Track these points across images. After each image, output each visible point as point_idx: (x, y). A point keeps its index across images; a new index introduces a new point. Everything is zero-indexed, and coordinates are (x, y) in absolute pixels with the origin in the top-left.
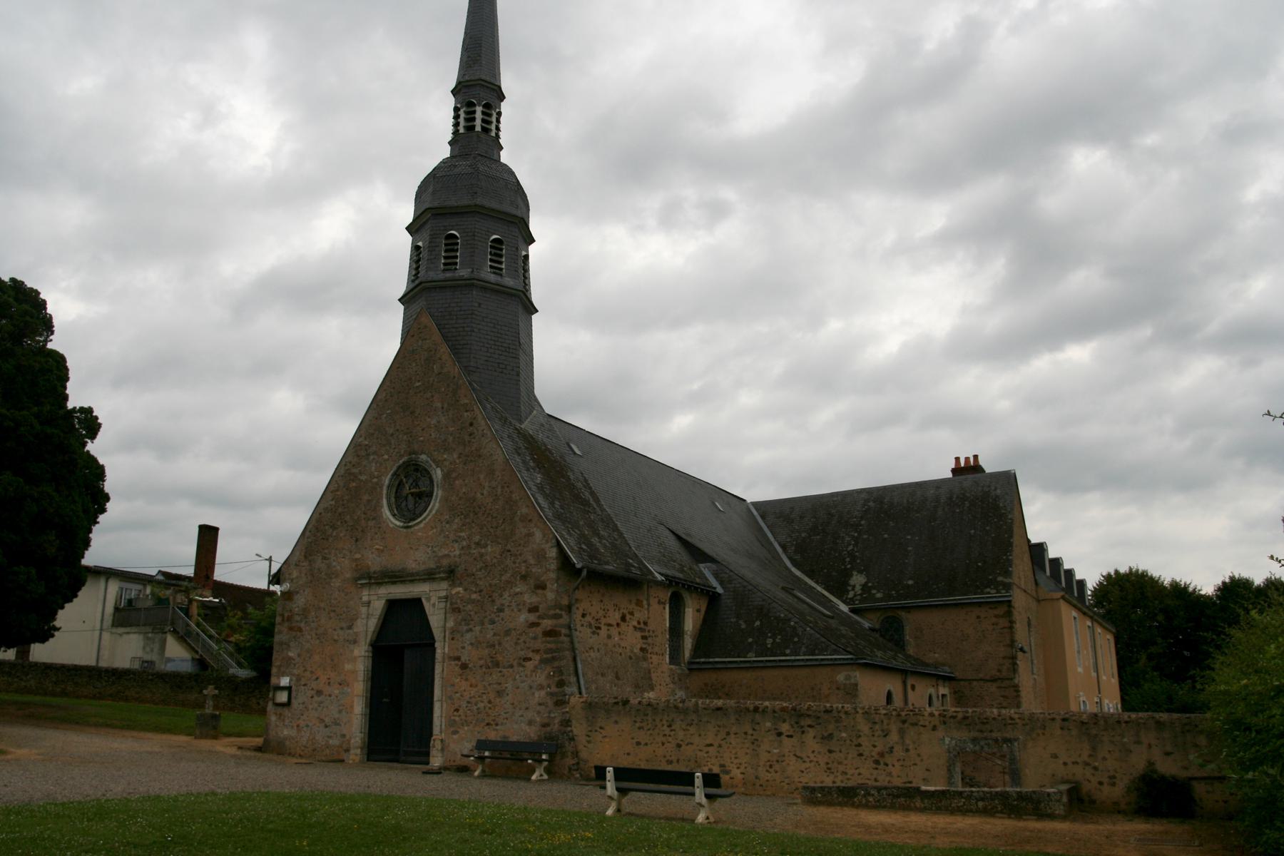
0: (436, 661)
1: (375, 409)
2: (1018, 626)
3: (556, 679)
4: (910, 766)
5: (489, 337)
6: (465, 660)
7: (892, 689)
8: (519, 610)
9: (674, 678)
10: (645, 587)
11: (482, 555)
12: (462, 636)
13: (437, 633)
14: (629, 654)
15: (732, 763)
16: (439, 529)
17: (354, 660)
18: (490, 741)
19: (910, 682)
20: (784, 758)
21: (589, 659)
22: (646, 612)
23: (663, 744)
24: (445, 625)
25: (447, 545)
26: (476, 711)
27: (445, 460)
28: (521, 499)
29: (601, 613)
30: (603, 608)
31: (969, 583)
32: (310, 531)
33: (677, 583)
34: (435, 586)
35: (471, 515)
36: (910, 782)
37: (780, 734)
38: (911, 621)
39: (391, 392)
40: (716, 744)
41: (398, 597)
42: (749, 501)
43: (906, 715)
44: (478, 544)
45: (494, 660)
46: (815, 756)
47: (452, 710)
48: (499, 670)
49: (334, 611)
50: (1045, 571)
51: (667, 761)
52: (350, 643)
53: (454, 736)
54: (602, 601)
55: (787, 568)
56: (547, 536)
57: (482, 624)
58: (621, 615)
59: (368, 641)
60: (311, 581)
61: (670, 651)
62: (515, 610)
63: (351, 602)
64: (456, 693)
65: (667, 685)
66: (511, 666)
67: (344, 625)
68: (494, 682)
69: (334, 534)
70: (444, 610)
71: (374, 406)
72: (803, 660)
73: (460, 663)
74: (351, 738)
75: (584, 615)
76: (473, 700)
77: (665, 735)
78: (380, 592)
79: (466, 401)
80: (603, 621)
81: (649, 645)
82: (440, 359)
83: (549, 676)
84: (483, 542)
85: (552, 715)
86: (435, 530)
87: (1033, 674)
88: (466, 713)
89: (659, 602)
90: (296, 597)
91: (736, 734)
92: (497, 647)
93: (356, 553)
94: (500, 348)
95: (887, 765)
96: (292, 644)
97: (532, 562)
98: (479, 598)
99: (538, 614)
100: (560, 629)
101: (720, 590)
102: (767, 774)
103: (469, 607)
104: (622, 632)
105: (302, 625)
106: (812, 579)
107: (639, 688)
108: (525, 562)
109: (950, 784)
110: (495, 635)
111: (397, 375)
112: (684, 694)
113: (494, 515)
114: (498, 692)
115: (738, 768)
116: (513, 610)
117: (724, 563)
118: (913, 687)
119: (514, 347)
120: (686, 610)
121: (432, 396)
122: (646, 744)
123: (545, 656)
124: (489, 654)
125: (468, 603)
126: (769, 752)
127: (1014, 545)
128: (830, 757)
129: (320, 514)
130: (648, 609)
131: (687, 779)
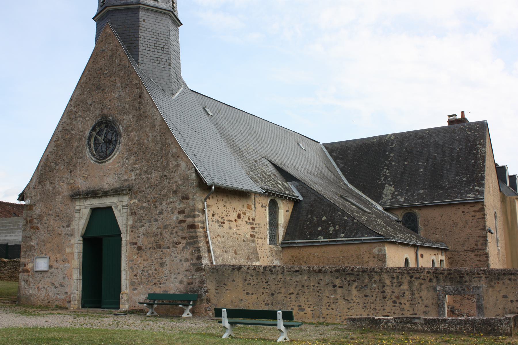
0: (122, 245)
1: (80, 89)
2: (488, 217)
3: (196, 255)
4: (415, 304)
5: (151, 41)
6: (140, 245)
7: (408, 257)
8: (173, 213)
9: (272, 253)
10: (253, 197)
11: (149, 179)
12: (138, 229)
13: (122, 228)
14: (243, 239)
15: (305, 304)
16: (121, 164)
17: (72, 246)
18: (157, 294)
19: (420, 252)
20: (337, 301)
21: (217, 242)
22: (254, 212)
23: (263, 293)
24: (127, 223)
25: (127, 173)
26: (147, 276)
27: (124, 120)
28: (172, 143)
29: (225, 213)
30: (226, 210)
31: (477, 194)
32: (42, 167)
33: (273, 194)
34: (120, 198)
35: (142, 154)
36: (416, 314)
37: (334, 286)
38: (422, 215)
39: (89, 78)
40: (295, 293)
41: (98, 206)
42: (321, 143)
43: (413, 273)
44: (146, 172)
45: (158, 244)
46: (356, 299)
47: (133, 275)
48: (161, 250)
49: (58, 216)
50: (506, 183)
51: (266, 304)
52: (69, 236)
53: (135, 292)
54: (225, 206)
55: (345, 184)
56: (189, 166)
57: (150, 221)
58: (237, 214)
59: (80, 234)
60: (44, 198)
61: (270, 235)
62: (170, 213)
63: (69, 210)
64: (135, 265)
65: (268, 257)
66: (169, 248)
67: (65, 225)
68: (158, 258)
69: (57, 168)
70: (126, 214)
71: (79, 86)
72: (352, 240)
73: (137, 246)
74: (71, 294)
75: (213, 215)
76: (146, 269)
77: (264, 288)
78: (86, 204)
79: (136, 82)
80: (226, 218)
81: (256, 233)
82: (120, 56)
83: (192, 254)
84: (149, 171)
85: (194, 277)
86: (119, 164)
87: (497, 246)
88: (142, 277)
89: (262, 206)
90: (34, 208)
91: (307, 286)
92: (159, 236)
93: (70, 179)
94: (158, 48)
95: (400, 303)
96: (33, 237)
97: (180, 182)
98: (148, 205)
99: (184, 215)
100: (198, 224)
101: (301, 198)
102: (327, 310)
103: (142, 211)
104: (238, 225)
105: (39, 225)
106: (360, 191)
107: (250, 259)
108: (176, 182)
109: (438, 313)
110: (158, 228)
111: (93, 67)
112: (279, 263)
113: (156, 153)
114: (161, 264)
115: (309, 307)
116: (168, 213)
117: (303, 181)
118: (422, 256)
119: (167, 47)
120: (280, 211)
121: (115, 80)
122: (252, 294)
123: (189, 241)
124: (155, 241)
125: (141, 209)
126: (328, 297)
127: (486, 167)
128: (365, 300)
129: (48, 155)
130: (255, 210)
131: (273, 315)
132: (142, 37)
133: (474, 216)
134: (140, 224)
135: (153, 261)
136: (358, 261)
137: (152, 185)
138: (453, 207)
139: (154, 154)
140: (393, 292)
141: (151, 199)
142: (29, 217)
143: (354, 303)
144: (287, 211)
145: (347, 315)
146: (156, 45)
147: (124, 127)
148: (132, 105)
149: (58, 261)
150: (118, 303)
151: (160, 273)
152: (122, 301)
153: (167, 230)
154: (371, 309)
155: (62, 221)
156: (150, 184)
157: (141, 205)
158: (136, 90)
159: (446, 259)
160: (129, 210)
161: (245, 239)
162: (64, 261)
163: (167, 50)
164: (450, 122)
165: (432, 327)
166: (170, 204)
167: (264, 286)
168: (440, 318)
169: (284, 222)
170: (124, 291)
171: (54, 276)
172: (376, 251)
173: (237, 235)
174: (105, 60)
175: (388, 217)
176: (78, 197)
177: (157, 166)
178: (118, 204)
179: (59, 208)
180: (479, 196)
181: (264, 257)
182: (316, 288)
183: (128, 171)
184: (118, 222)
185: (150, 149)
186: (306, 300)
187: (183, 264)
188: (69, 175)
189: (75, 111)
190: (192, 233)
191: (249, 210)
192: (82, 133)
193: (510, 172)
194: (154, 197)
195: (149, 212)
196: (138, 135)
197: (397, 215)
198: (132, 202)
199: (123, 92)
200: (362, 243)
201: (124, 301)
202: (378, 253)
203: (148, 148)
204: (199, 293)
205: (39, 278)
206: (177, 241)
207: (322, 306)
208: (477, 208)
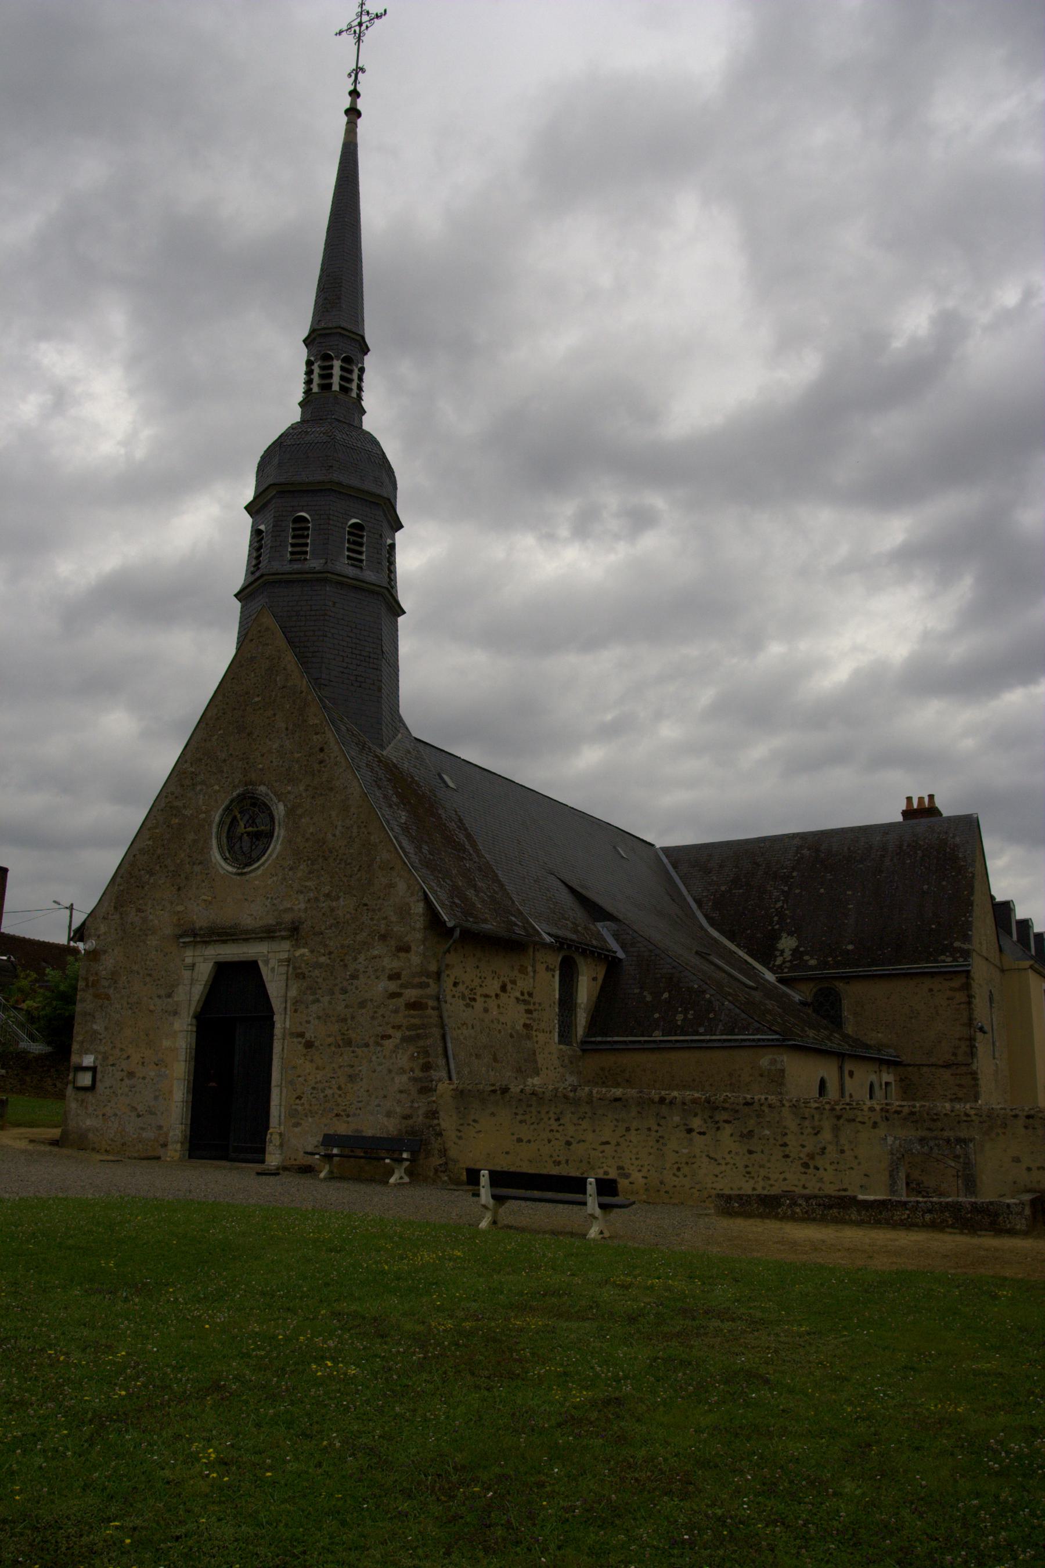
0: (275, 1037)
2: (977, 1001)
5: (345, 644)
7: (826, 1076)
9: (563, 1061)
10: (531, 950)
11: (332, 910)
13: (276, 1004)
14: (510, 1031)
15: (632, 1164)
16: (280, 877)
19: (848, 1067)
21: (462, 1038)
22: (531, 981)
23: (549, 1141)
24: (286, 993)
25: (290, 896)
27: (289, 792)
28: (381, 842)
30: (479, 975)
32: (122, 877)
33: (569, 947)
34: (275, 946)
36: (845, 1190)
37: (690, 1131)
38: (851, 994)
39: (223, 709)
40: (613, 1142)
41: (229, 959)
43: (841, 1109)
44: (327, 896)
46: (732, 1158)
48: (351, 1049)
51: (554, 1162)
53: (296, 1130)
55: (702, 927)
57: (332, 993)
59: (192, 1013)
62: (373, 977)
65: (555, 1068)
66: (367, 1045)
69: (152, 881)
70: (284, 977)
72: (719, 1040)
73: (304, 1041)
75: (455, 984)
76: (320, 1086)
77: (552, 1131)
78: (206, 953)
80: (479, 991)
81: (534, 1020)
85: (416, 1105)
87: (994, 1058)
89: (548, 969)
92: (349, 1021)
93: (177, 904)
98: (328, 961)
99: (399, 982)
101: (621, 954)
102: (675, 1178)
103: (317, 972)
104: (501, 1005)
105: (111, 991)
108: (386, 918)
110: (346, 1007)
115: (640, 1171)
118: (851, 1074)
120: (580, 978)
121: (275, 715)
122: (529, 1141)
123: (407, 1033)
124: (340, 1031)
126: (677, 1152)
127: (975, 904)
130: (534, 978)
131: (578, 1185)
133: (952, 1000)
134: (311, 998)
135: (334, 1070)
136: (729, 1082)
137: (338, 922)
138: (911, 979)
139: (345, 862)
140: (803, 1146)
141: (337, 947)
142: (92, 974)
143: (727, 1164)
144: (595, 979)
145: (712, 1188)
146: (354, 651)
147: (289, 806)
148: (305, 765)
149: (145, 1064)
150: (263, 1151)
151: (348, 1094)
152: (270, 1148)
153: (364, 1011)
154: (760, 1178)
155: (157, 985)
156: (335, 919)
157: (315, 960)
158: (315, 737)
159: (895, 1081)
160: (291, 968)
161: (513, 1033)
162: (157, 1065)
163: (375, 661)
164: (908, 814)
165: (879, 1217)
166: (373, 961)
167: (553, 1128)
168: (895, 1198)
169: (588, 999)
170: (275, 1128)
171: (136, 1092)
172: (766, 1064)
173: (499, 1023)
174: (255, 676)
175: (787, 995)
176: (192, 939)
177: (349, 885)
178: (270, 955)
179: (153, 960)
180: (961, 960)
181: (547, 1068)
182: (653, 1134)
183: (292, 893)
184: (269, 992)
185: (337, 851)
186: (633, 1157)
187: (393, 1078)
188: (176, 896)
189: (193, 772)
190: (415, 1018)
191: (523, 976)
192: (204, 815)
193: (1037, 929)
194: (342, 946)
195: (332, 973)
196: (314, 824)
197: (803, 992)
198: (297, 954)
199: (289, 739)
200: (741, 1046)
201: (274, 1148)
202: (769, 1067)
203: (333, 850)
204: (424, 1136)
205: (107, 1096)
206: (383, 1033)
207: (665, 1169)
208: (957, 983)
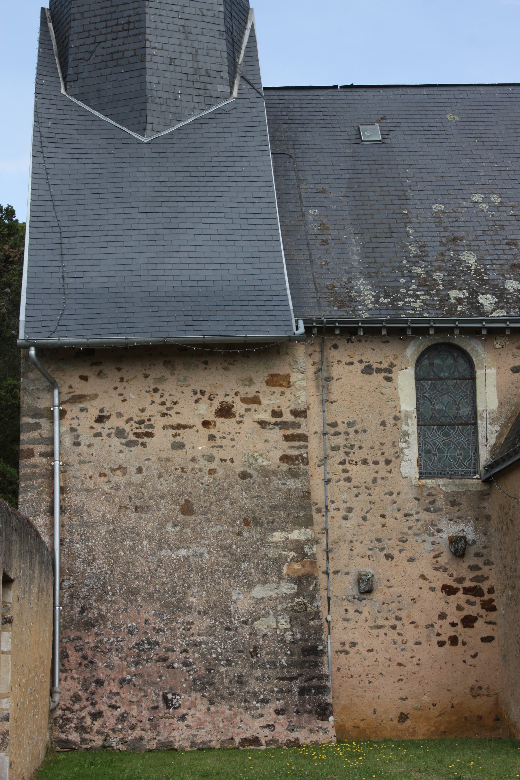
100: (31, 446)
132: (78, 16)
